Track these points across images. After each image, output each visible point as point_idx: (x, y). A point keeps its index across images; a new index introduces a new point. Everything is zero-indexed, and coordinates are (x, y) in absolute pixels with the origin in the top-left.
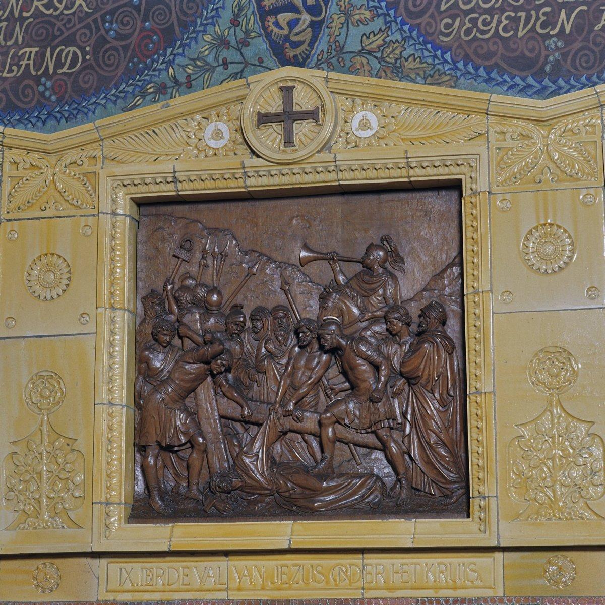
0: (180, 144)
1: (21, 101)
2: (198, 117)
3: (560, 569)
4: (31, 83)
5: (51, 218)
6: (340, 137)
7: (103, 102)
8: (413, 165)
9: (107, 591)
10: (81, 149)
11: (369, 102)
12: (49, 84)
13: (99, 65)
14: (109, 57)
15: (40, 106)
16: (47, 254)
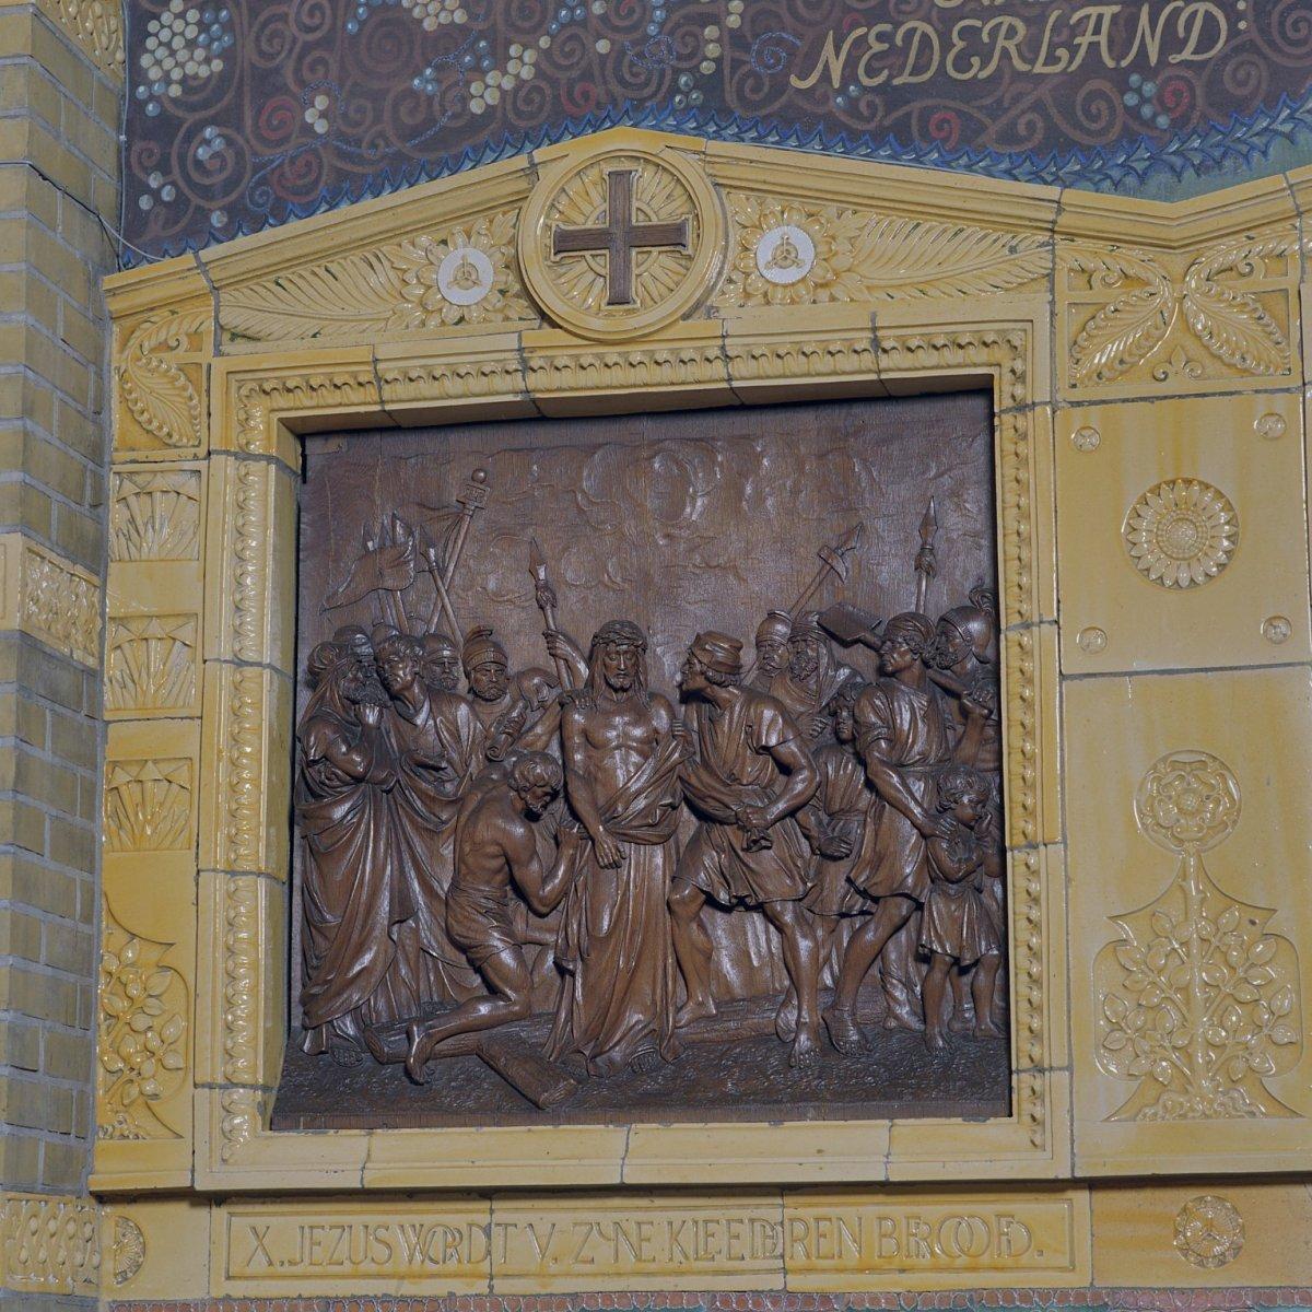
0: (387, 297)
1: (1082, 128)
2: (424, 240)
3: (1209, 1225)
4: (1106, 86)
5: (1180, 397)
6: (730, 281)
7: (1287, 128)
8: (887, 344)
9: (228, 1278)
10: (1249, 238)
11: (796, 205)
12: (1149, 89)
13: (1272, 44)
14: (1296, 23)
15: (1131, 139)
16: (1174, 482)
